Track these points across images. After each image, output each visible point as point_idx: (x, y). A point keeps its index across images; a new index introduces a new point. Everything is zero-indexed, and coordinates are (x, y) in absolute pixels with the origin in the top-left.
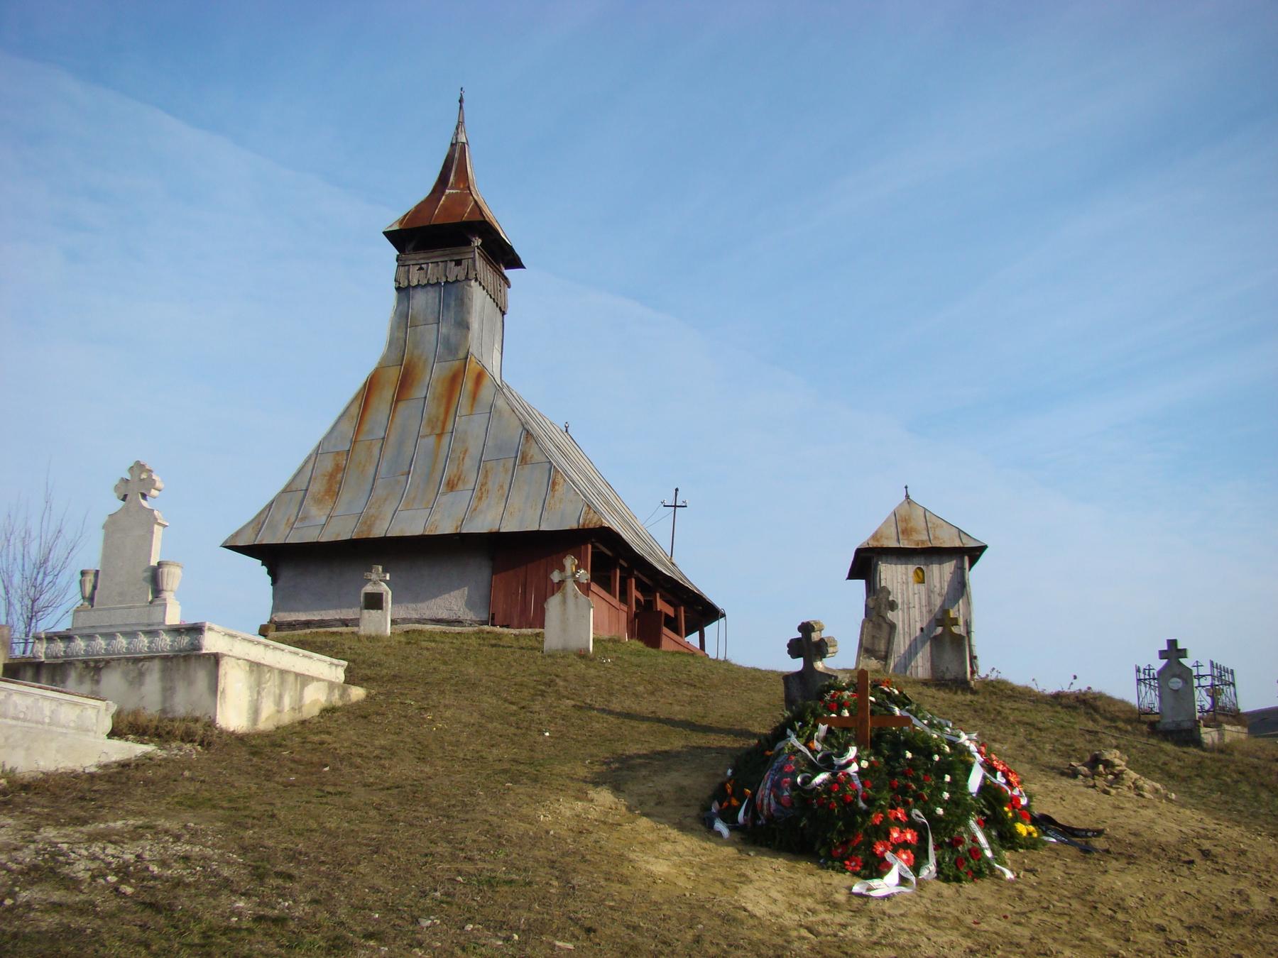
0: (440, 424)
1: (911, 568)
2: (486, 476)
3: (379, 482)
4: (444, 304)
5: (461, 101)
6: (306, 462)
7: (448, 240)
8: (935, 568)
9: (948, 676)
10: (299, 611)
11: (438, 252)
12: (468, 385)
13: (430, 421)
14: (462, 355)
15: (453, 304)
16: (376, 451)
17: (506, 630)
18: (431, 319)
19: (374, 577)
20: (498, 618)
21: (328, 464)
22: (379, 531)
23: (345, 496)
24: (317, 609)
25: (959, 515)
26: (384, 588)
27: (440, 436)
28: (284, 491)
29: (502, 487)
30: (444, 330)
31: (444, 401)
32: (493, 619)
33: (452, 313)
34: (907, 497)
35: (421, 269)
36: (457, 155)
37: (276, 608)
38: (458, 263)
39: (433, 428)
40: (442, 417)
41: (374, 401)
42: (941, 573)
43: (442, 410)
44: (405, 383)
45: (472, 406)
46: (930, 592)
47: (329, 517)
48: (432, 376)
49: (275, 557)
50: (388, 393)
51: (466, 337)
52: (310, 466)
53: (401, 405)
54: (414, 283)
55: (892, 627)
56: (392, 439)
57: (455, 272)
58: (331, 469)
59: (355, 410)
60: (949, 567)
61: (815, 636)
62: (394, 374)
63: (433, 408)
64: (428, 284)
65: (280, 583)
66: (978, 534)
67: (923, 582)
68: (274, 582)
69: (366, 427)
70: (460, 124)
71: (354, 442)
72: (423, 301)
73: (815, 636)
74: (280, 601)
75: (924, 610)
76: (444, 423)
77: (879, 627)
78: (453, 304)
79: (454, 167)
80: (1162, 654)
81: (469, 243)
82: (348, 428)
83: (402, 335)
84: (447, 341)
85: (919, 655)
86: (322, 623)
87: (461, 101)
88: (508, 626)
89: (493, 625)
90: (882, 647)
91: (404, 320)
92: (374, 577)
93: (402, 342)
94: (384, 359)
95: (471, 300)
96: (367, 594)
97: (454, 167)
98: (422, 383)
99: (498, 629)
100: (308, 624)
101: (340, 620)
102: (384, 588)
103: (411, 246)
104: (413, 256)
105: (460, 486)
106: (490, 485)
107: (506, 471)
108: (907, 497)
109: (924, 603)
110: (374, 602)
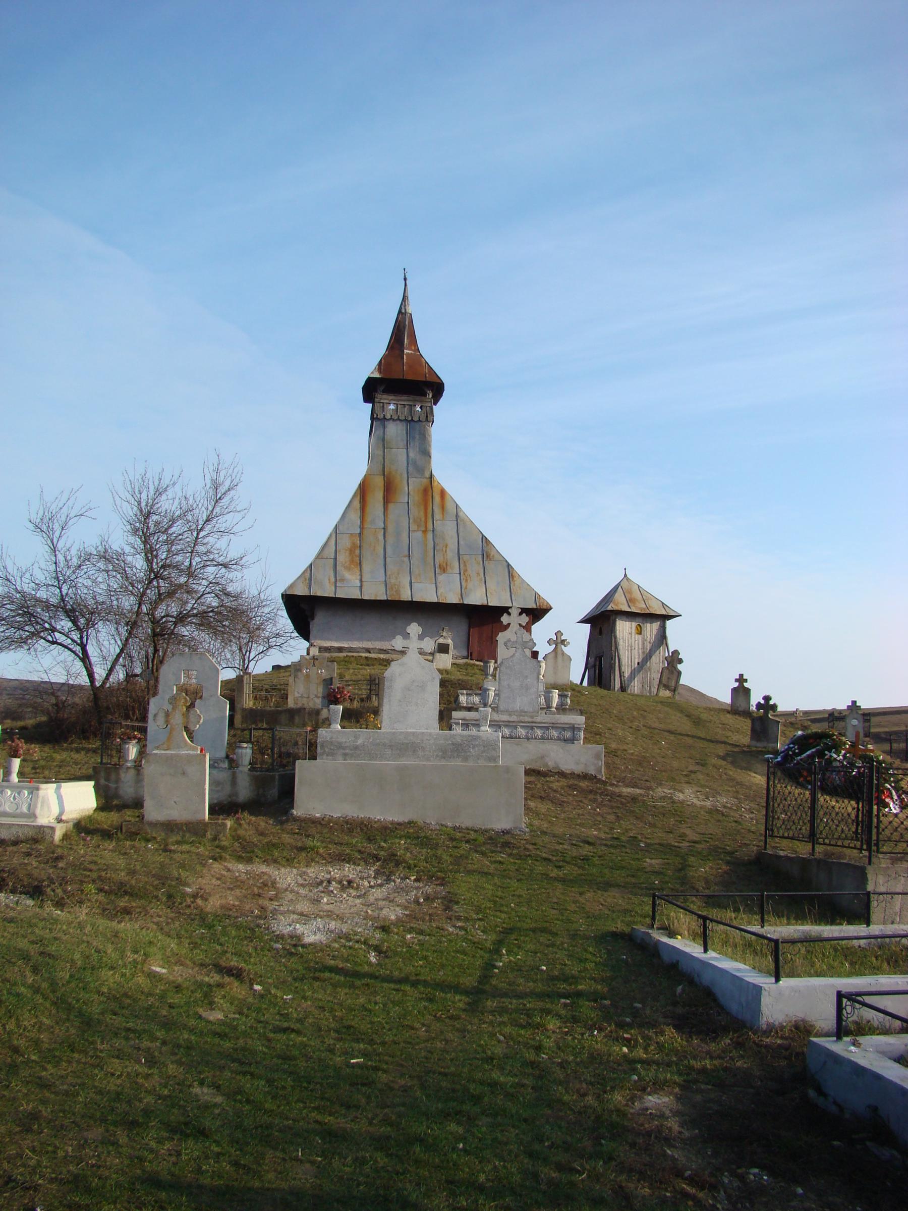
0: (423, 524)
1: (634, 624)
2: (465, 565)
3: (388, 559)
5: (405, 279)
7: (403, 386)
8: (648, 625)
9: (740, 709)
10: (331, 640)
12: (437, 499)
13: (415, 521)
14: (427, 475)
15: (417, 437)
16: (381, 538)
17: (478, 663)
20: (475, 655)
21: (345, 542)
22: (406, 596)
23: (366, 567)
25: (660, 589)
26: (450, 641)
30: (411, 455)
31: (422, 507)
33: (417, 444)
34: (625, 575)
39: (419, 526)
40: (423, 519)
41: (370, 499)
42: (651, 629)
43: (422, 513)
44: (389, 490)
46: (644, 640)
47: (361, 581)
50: (379, 495)
51: (429, 462)
52: (333, 541)
53: (391, 506)
55: (679, 673)
56: (391, 529)
59: (357, 504)
60: (656, 625)
61: (771, 702)
62: (379, 481)
63: (416, 512)
64: (398, 419)
66: (674, 605)
67: (640, 634)
69: (368, 518)
70: (405, 298)
71: (362, 527)
73: (771, 702)
75: (640, 651)
76: (426, 522)
77: (672, 673)
78: (417, 437)
79: (402, 332)
80: (736, 680)
81: (425, 395)
82: (355, 517)
84: (415, 463)
85: (636, 679)
86: (351, 650)
87: (405, 279)
90: (673, 684)
92: (444, 634)
95: (430, 437)
96: (439, 644)
97: (402, 332)
98: (398, 489)
100: (340, 650)
104: (385, 396)
105: (449, 570)
106: (470, 572)
107: (478, 563)
108: (625, 575)
109: (640, 647)
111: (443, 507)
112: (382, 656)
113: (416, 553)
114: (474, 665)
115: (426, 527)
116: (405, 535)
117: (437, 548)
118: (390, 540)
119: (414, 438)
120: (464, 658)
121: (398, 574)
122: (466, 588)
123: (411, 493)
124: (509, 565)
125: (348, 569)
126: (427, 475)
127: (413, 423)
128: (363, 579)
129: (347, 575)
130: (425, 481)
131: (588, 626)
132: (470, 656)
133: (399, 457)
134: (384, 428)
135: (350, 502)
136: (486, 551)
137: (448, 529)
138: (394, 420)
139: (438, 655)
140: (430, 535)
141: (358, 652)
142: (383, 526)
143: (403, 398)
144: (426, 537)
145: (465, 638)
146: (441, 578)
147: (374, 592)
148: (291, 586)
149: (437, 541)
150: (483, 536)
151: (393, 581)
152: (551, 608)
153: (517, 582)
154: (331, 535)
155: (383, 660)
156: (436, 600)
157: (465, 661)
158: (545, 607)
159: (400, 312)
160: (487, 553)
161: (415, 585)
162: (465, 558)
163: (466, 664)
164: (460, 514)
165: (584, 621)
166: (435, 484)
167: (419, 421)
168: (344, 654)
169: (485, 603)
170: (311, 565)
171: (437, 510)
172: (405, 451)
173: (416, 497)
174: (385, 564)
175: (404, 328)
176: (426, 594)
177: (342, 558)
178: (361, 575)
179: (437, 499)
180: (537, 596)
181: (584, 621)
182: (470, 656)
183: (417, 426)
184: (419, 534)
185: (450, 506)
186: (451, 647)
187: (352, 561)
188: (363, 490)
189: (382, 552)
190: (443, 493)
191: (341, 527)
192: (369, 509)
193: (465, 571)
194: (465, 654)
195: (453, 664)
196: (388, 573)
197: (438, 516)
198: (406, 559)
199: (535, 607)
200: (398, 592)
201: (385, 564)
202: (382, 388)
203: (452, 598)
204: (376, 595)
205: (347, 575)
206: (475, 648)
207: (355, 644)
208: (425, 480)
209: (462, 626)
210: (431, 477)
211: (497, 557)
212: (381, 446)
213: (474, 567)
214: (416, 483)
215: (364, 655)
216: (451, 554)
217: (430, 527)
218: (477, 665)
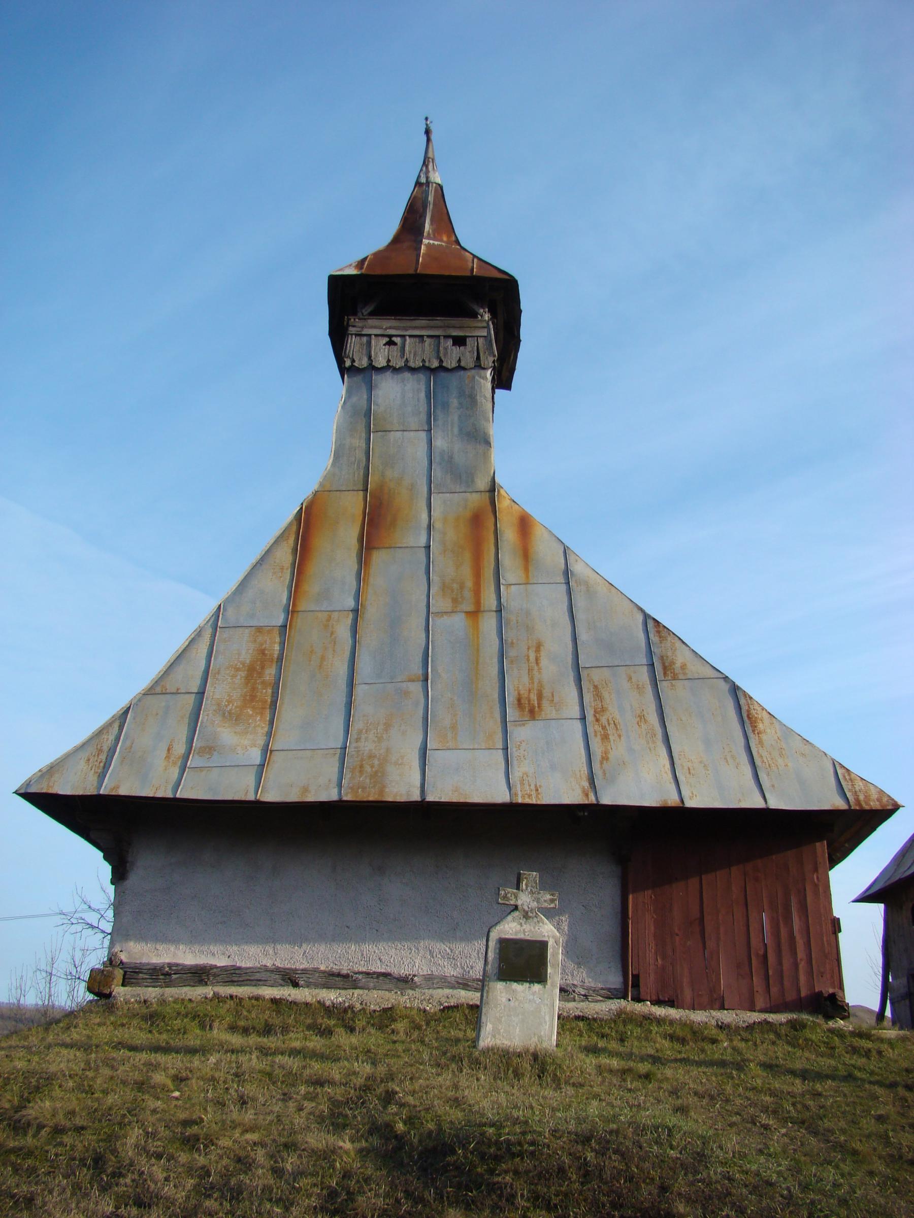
0: (468, 594)
2: (598, 695)
3: (359, 690)
4: (434, 408)
5: (428, 132)
6: (192, 642)
10: (175, 941)
11: (422, 322)
12: (509, 535)
13: (444, 587)
15: (454, 402)
16: (343, 631)
17: (660, 1011)
18: (416, 420)
19: (524, 899)
20: (649, 983)
21: (239, 648)
22: (403, 786)
23: (290, 713)
24: (217, 940)
27: (475, 614)
28: (150, 692)
29: (642, 718)
30: (440, 443)
31: (467, 556)
32: (636, 985)
35: (391, 343)
36: (431, 198)
37: (119, 933)
38: (460, 341)
39: (455, 601)
40: (469, 584)
41: (321, 543)
45: (526, 569)
47: (266, 751)
48: (430, 518)
49: (103, 819)
50: (349, 535)
51: (486, 457)
53: (379, 558)
54: (381, 362)
56: (373, 611)
57: (452, 355)
58: (250, 661)
59: (284, 556)
65: (133, 879)
68: (119, 876)
69: (312, 587)
70: (427, 161)
71: (291, 611)
72: (396, 394)
74: (128, 918)
78: (454, 402)
81: (474, 315)
82: (275, 587)
83: (360, 443)
84: (449, 462)
86: (234, 975)
87: (428, 132)
88: (671, 1003)
89: (638, 999)
91: (364, 420)
92: (524, 899)
93: (361, 455)
94: (329, 477)
96: (505, 944)
99: (646, 1008)
100: (200, 975)
101: (277, 970)
102: (547, 931)
103: (369, 309)
105: (548, 710)
106: (613, 711)
107: (639, 688)
110: (522, 962)
111: (526, 554)
112: (331, 996)
113: (447, 669)
114: (648, 1018)
115: (478, 602)
116: (416, 623)
117: (512, 653)
118: (370, 638)
119: (446, 406)
120: (612, 994)
121: (388, 726)
122: (605, 758)
123: (438, 525)
124: (735, 690)
125: (234, 718)
126: (482, 483)
127: (443, 374)
128: (276, 745)
129: (227, 735)
130: (476, 500)
131: (880, 907)
132: (632, 987)
133: (408, 453)
134: (370, 388)
135: (268, 552)
136: (659, 653)
137: (543, 606)
138: (396, 370)
139: (500, 990)
140: (489, 623)
141: (258, 982)
142: (350, 603)
143: (418, 323)
144: (476, 627)
145: (609, 927)
146: (524, 733)
147: (304, 777)
148: (51, 770)
149: (508, 635)
150: (646, 616)
151: (368, 746)
152: (896, 807)
153: (769, 735)
154: (199, 633)
155: (329, 1010)
156: (501, 796)
157: (615, 1005)
158: (875, 805)
159: (418, 184)
160: (662, 658)
161: (435, 758)
162: (597, 676)
163: (622, 1017)
164: (577, 568)
165: (868, 897)
166: (503, 505)
167: (460, 368)
168: (208, 991)
169: (672, 800)
170: (126, 712)
171: (509, 560)
172: (423, 435)
173: (449, 533)
174: (349, 704)
175: (425, 207)
176: (473, 778)
177: (217, 691)
178: (269, 734)
179: (509, 535)
180: (841, 776)
181: (868, 897)
182: (632, 987)
183: (453, 380)
184: (458, 621)
185: (545, 551)
186: (556, 955)
187: (251, 698)
188: (306, 525)
189: (342, 669)
190: (525, 524)
191: (230, 612)
192: (316, 567)
193: (600, 711)
194: (614, 980)
195: (565, 1021)
196: (357, 725)
197: (511, 572)
198: (416, 688)
199: (841, 804)
200: (378, 776)
201: (349, 704)
202: (369, 309)
203: (562, 789)
204: (305, 790)
205: (227, 735)
206: (649, 960)
207: (250, 955)
208: (476, 497)
209: (600, 889)
210: (493, 488)
211: (695, 668)
212: (361, 427)
213: (628, 700)
214: (450, 507)
215: (269, 992)
216: (554, 668)
217: (489, 600)
218: (659, 1021)
